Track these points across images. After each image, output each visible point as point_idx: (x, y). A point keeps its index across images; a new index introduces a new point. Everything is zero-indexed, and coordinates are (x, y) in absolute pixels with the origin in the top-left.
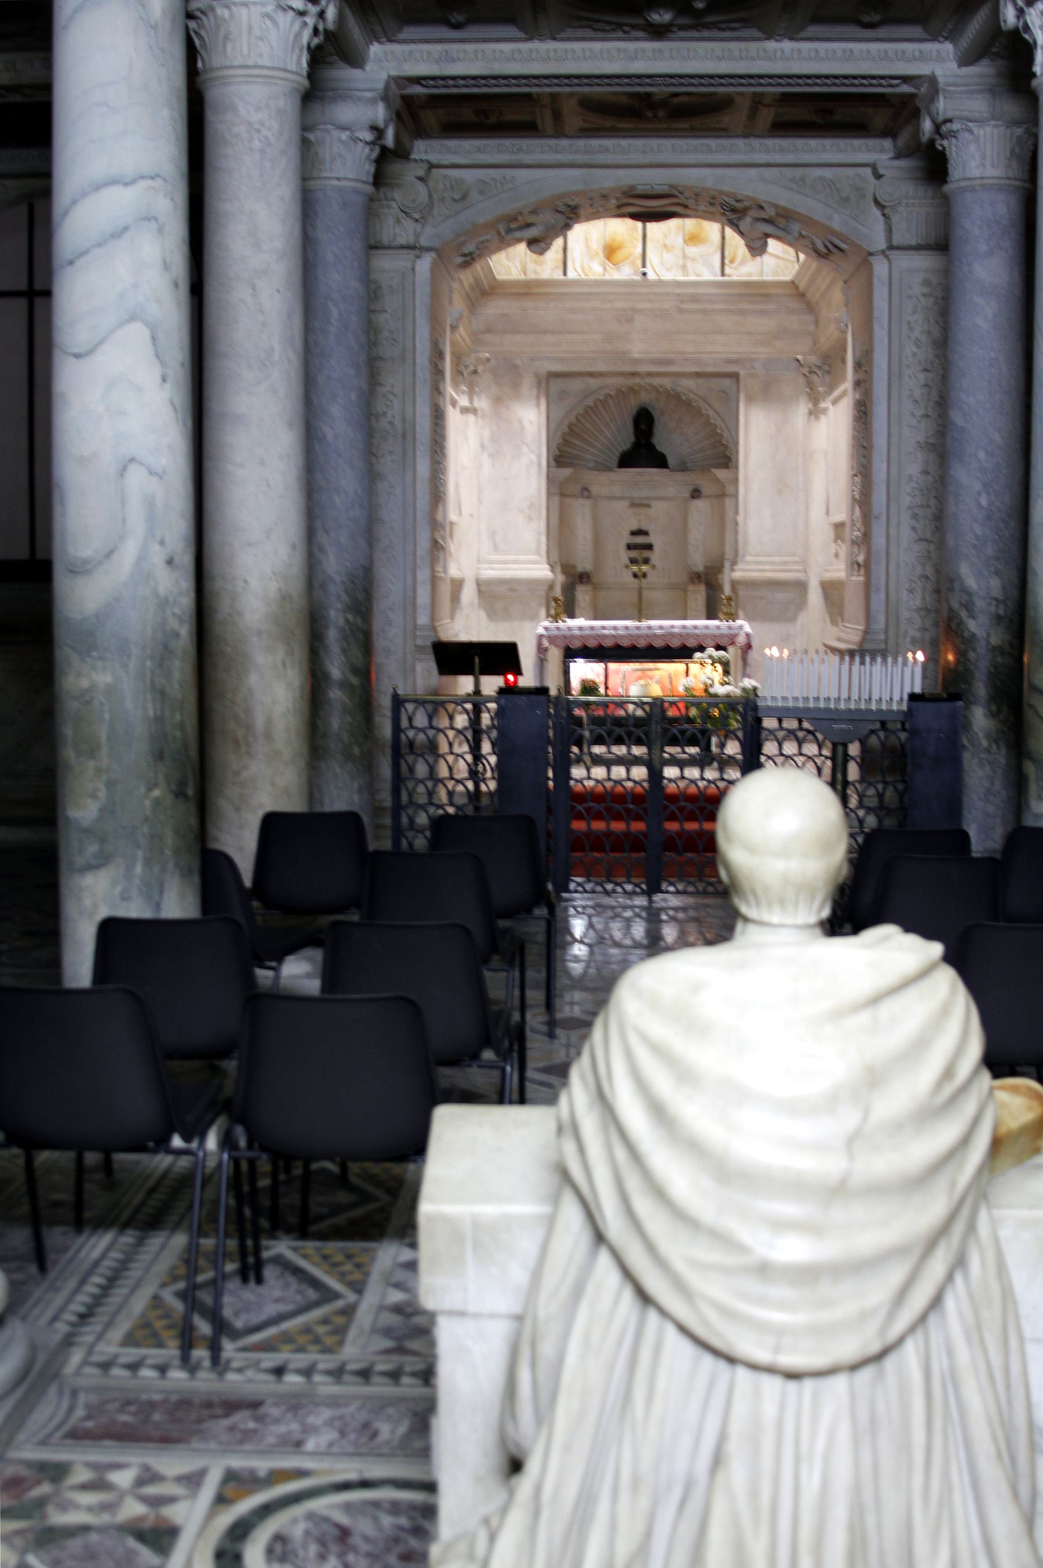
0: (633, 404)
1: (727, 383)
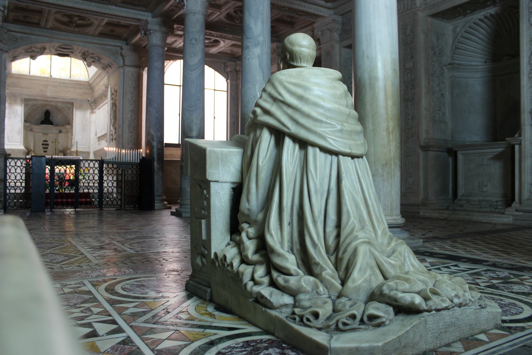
1: (70, 105)
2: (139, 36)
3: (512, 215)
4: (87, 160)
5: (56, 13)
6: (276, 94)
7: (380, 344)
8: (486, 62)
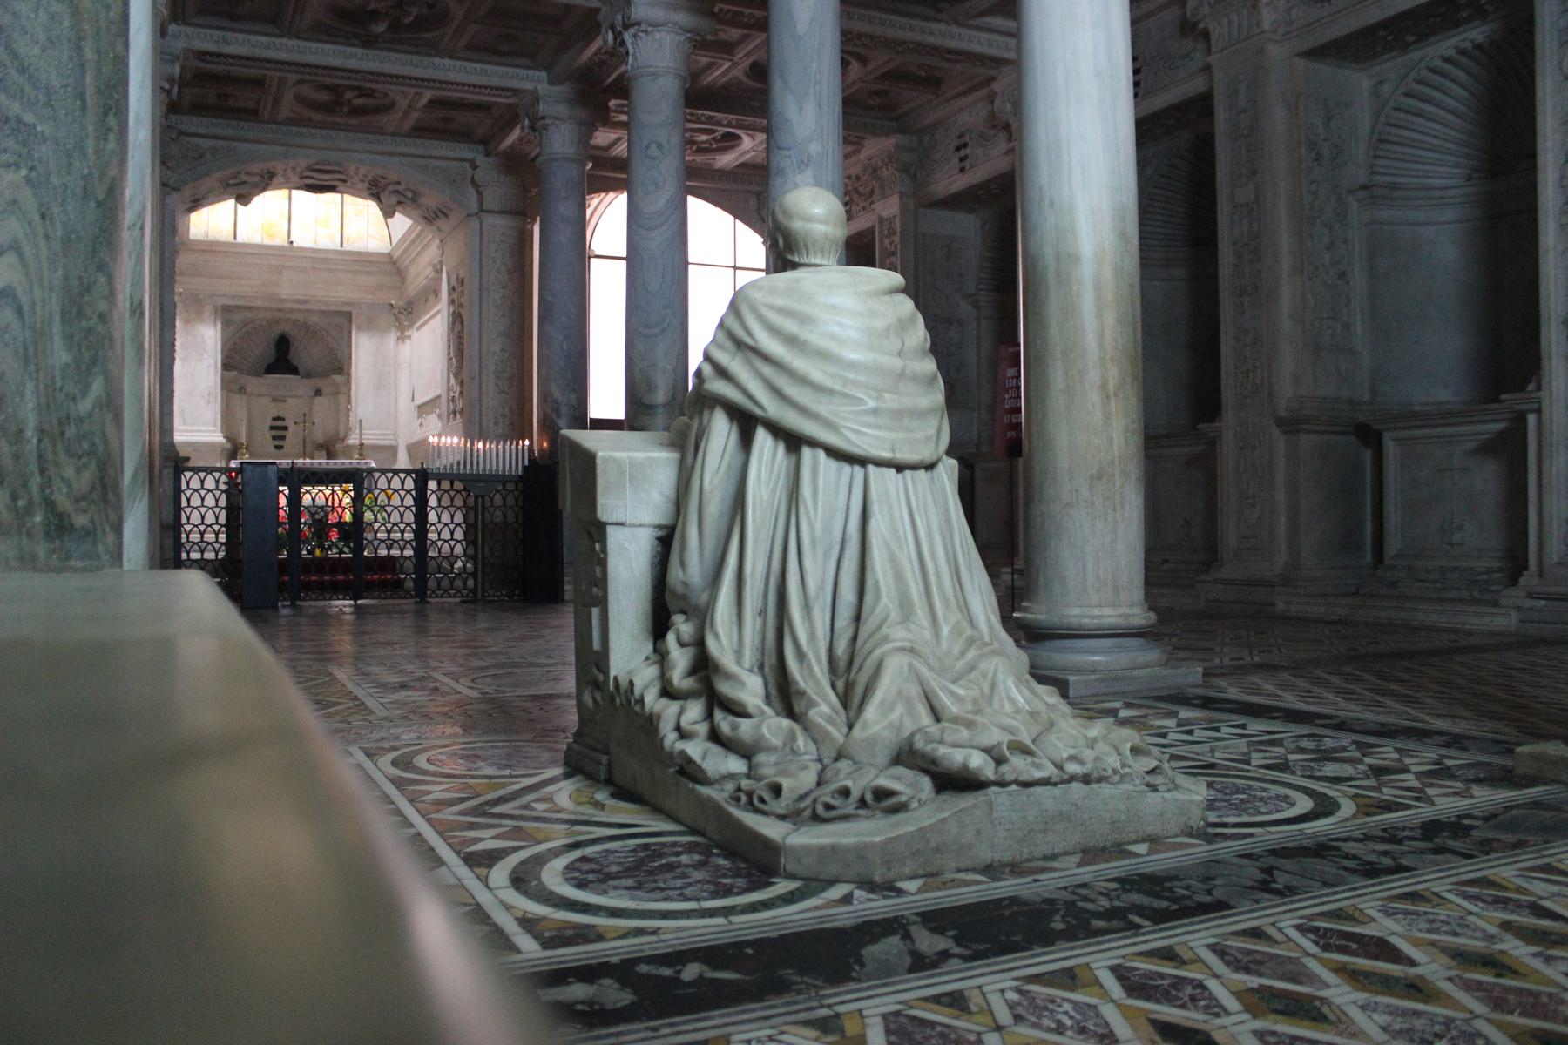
0: (276, 331)
1: (343, 320)
2: (516, 134)
3: (1519, 609)
4: (383, 471)
5: (300, 82)
6: (741, 333)
7: (878, 839)
8: (1470, 178)
